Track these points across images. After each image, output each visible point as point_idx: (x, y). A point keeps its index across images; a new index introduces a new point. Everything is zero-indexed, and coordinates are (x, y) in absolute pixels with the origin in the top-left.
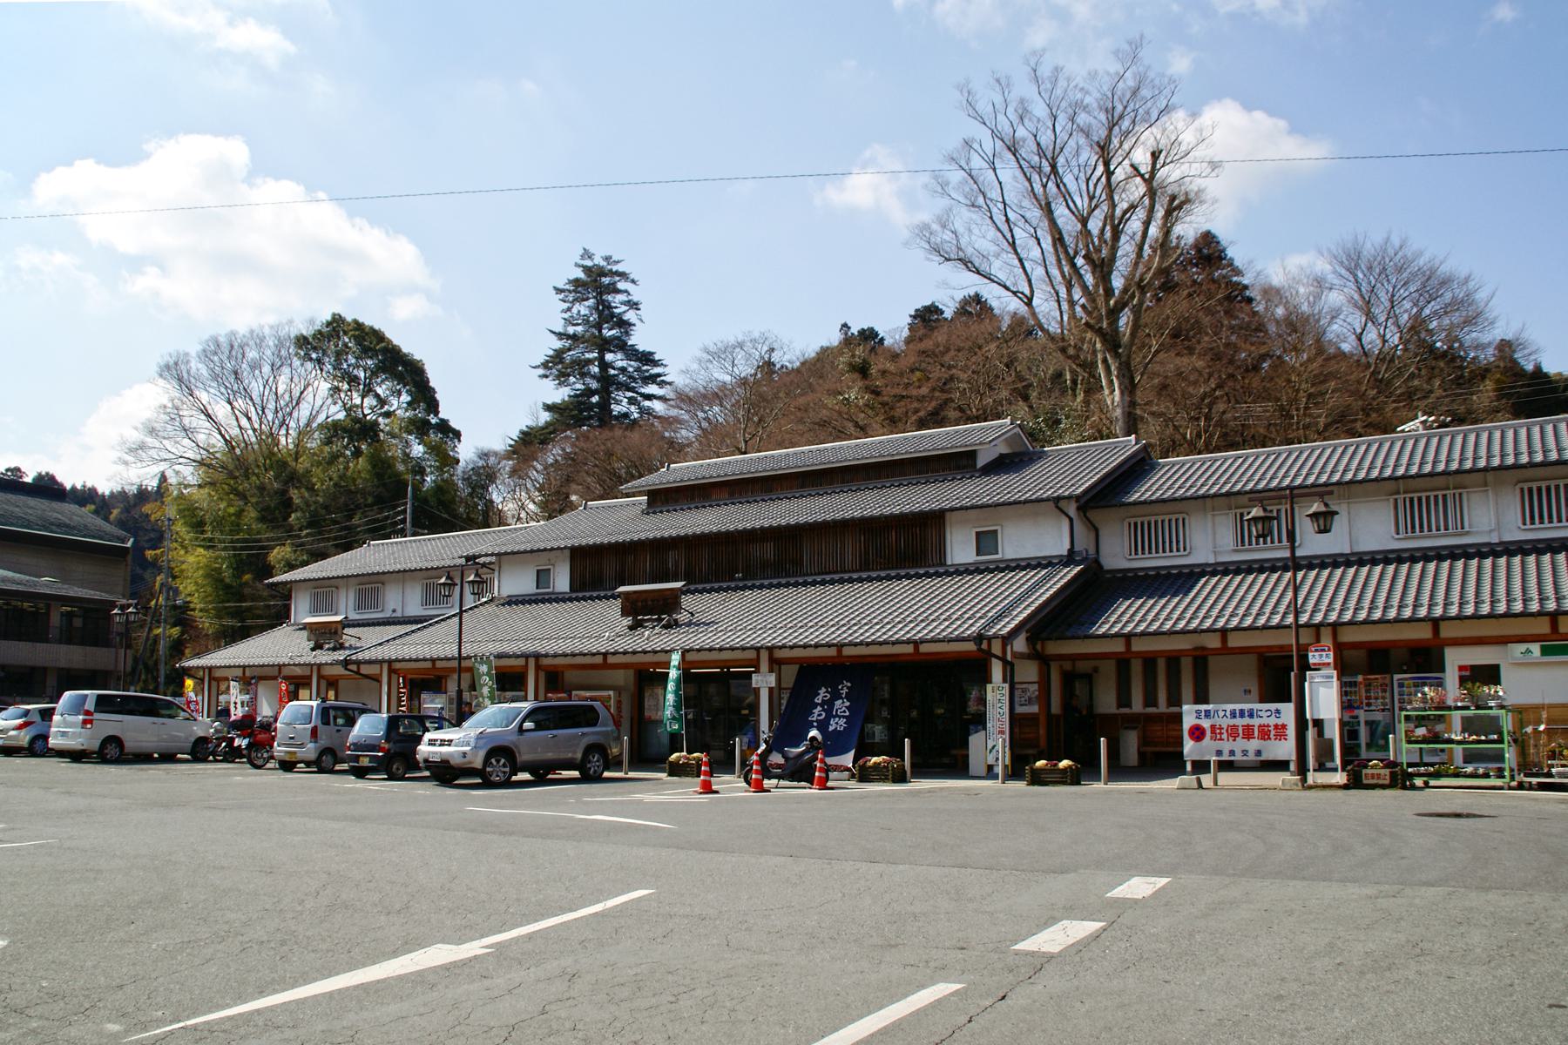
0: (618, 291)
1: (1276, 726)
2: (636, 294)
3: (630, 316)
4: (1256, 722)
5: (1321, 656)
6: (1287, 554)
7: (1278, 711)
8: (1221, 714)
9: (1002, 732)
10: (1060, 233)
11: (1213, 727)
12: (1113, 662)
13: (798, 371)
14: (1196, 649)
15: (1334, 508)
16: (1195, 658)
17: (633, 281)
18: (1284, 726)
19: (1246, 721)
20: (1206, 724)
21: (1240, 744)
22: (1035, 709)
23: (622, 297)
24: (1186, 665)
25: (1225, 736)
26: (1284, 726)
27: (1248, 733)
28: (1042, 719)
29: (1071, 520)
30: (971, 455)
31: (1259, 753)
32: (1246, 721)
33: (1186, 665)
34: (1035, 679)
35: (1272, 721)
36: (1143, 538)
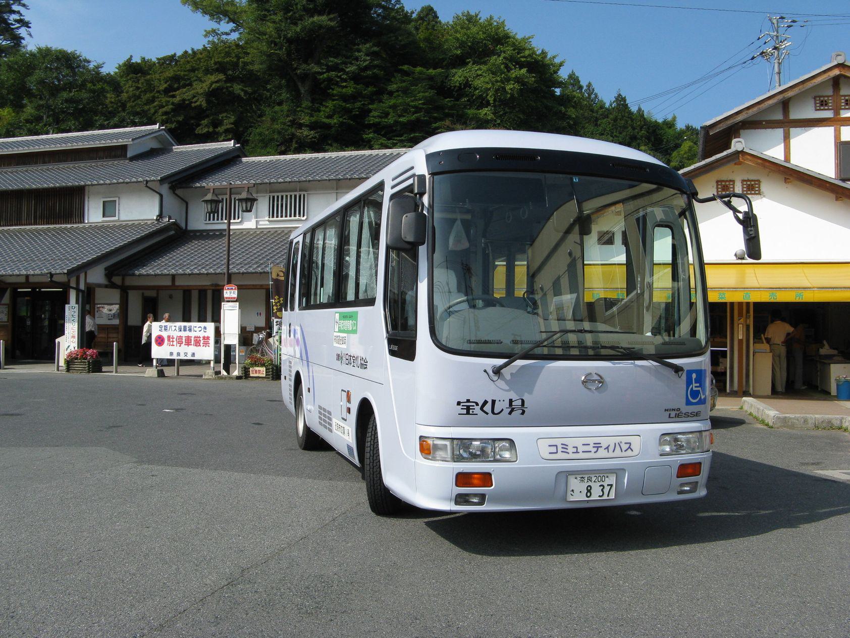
0: (14, 12)
1: (204, 338)
2: (27, 16)
3: (23, 32)
4: (192, 334)
5: (230, 293)
6: (225, 227)
7: (205, 328)
8: (173, 328)
9: (73, 337)
10: (785, 140)
11: (169, 337)
12: (181, 292)
13: (112, 82)
14: (212, 285)
15: (255, 195)
16: (214, 291)
17: (24, 5)
18: (208, 338)
19: (187, 333)
20: (165, 334)
21: (176, 349)
22: (116, 322)
23: (17, 17)
24: (195, 295)
25: (175, 343)
26: (208, 338)
27: (188, 342)
28: (121, 328)
29: (161, 196)
30: (124, 148)
31: (193, 354)
32: (187, 333)
33: (195, 295)
34: (118, 302)
35: (202, 334)
36: (214, 210)
